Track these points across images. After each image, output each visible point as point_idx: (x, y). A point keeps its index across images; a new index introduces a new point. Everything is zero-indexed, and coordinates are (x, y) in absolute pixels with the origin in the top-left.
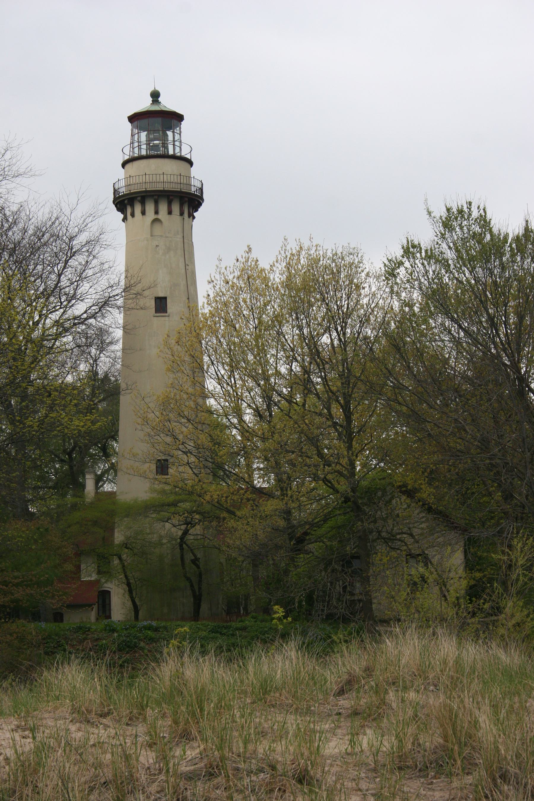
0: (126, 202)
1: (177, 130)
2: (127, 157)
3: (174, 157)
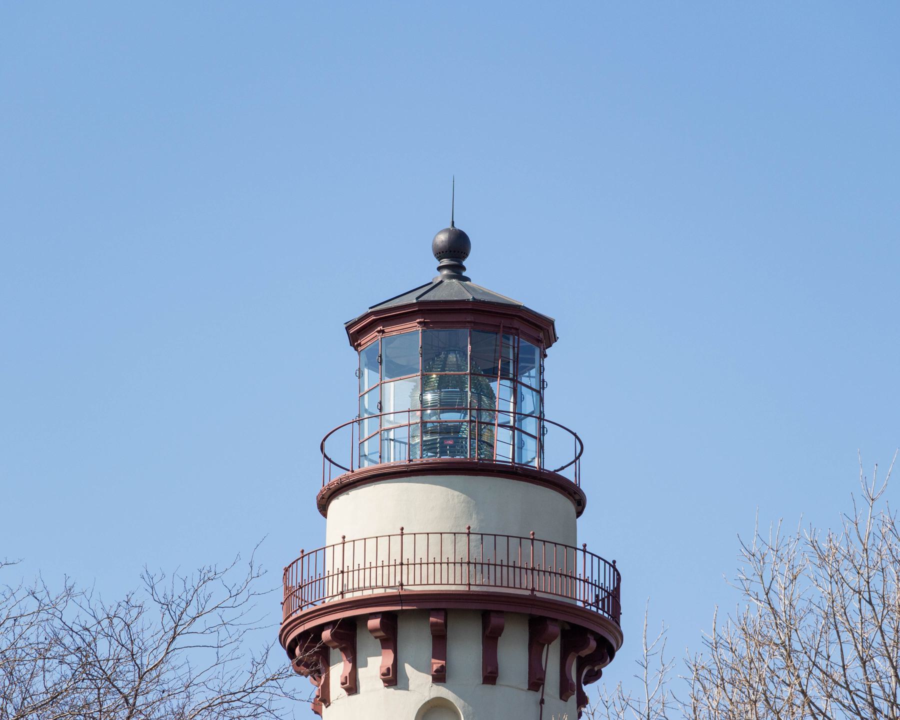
0: (326, 634)
1: (529, 379)
2: (337, 475)
3: (516, 472)
